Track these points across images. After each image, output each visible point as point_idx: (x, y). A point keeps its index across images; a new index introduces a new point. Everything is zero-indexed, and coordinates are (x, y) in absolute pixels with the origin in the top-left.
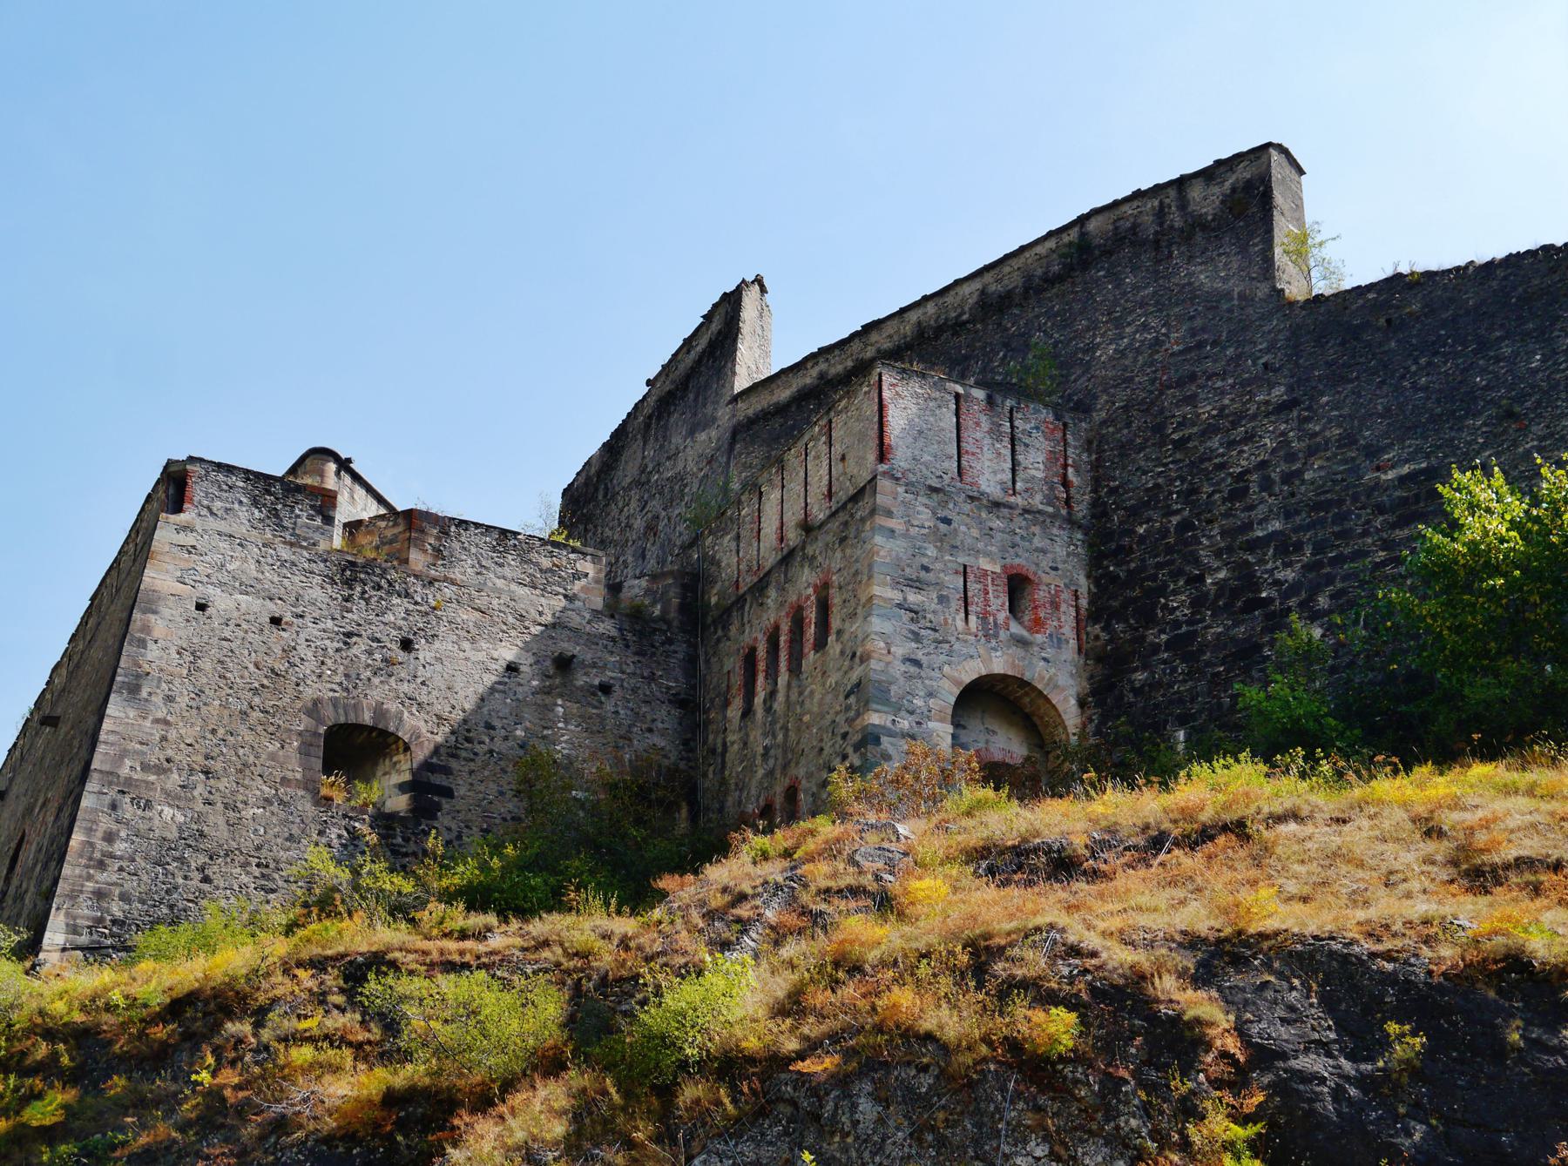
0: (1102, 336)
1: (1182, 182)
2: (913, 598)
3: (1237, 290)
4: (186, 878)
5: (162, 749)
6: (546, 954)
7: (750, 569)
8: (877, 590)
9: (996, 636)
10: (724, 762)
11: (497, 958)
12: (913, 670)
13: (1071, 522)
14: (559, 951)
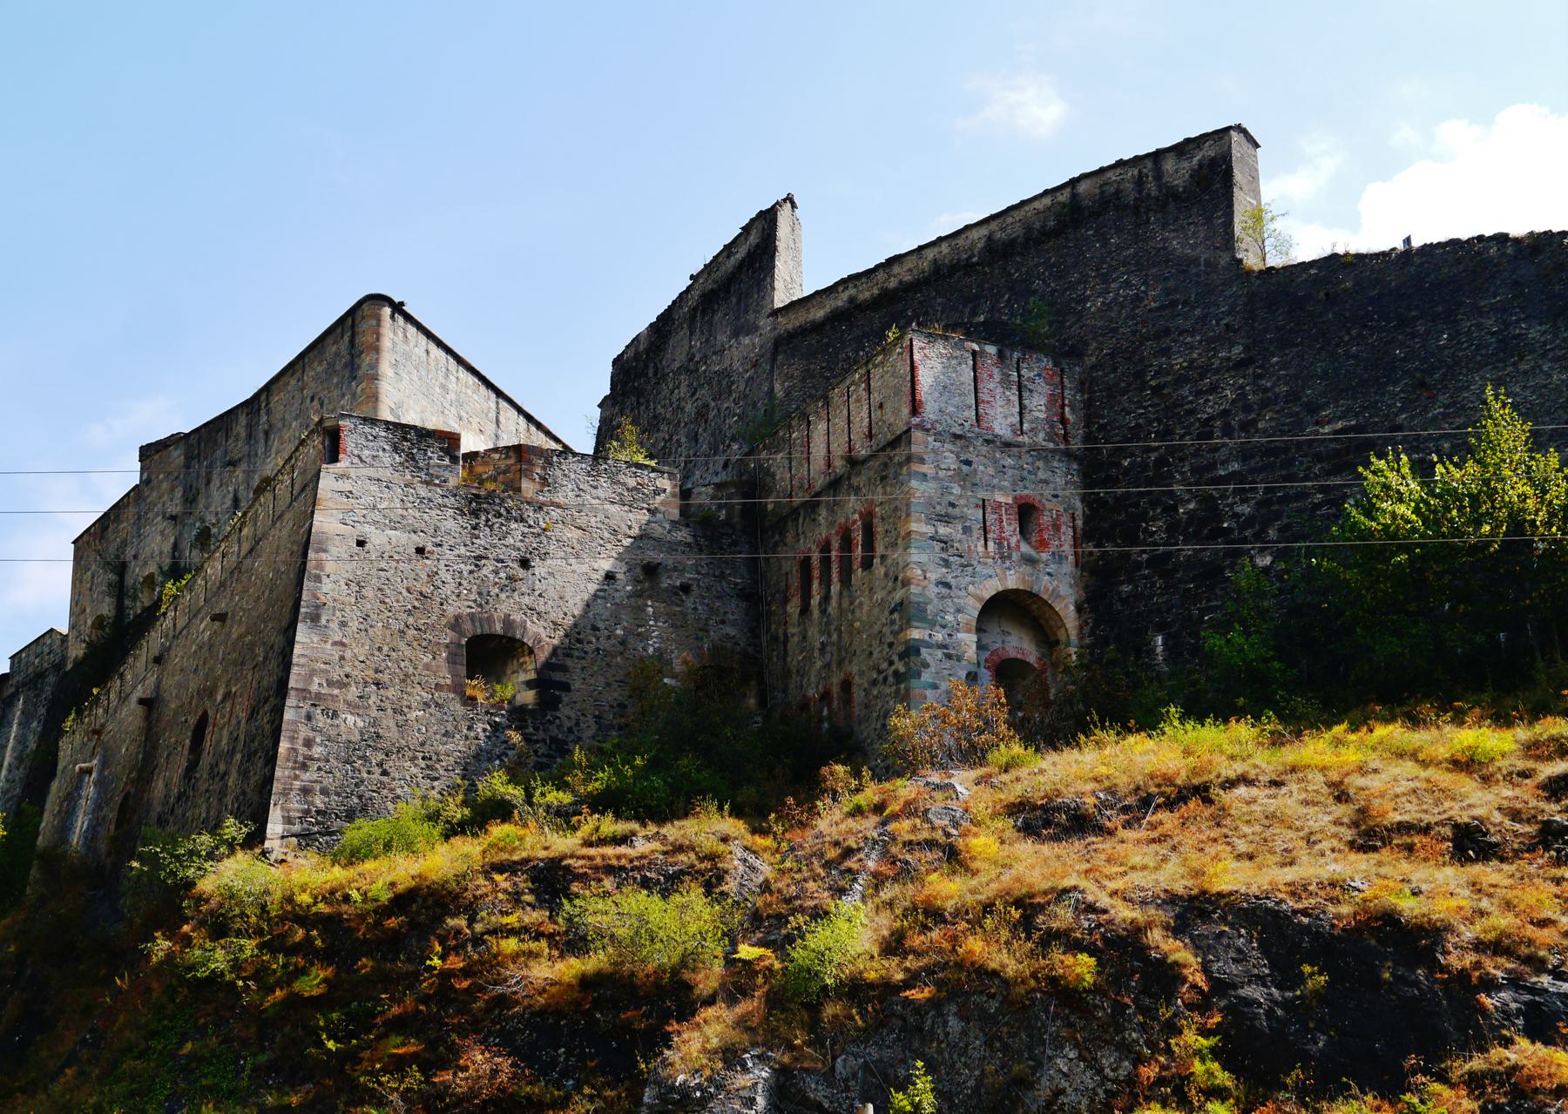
0: (1092, 288)
1: (1158, 155)
2: (943, 530)
3: (1203, 257)
4: (369, 772)
5: (342, 667)
6: (682, 857)
7: (801, 487)
8: (914, 526)
9: (1010, 557)
10: (786, 651)
11: (646, 862)
12: (945, 591)
13: (1069, 455)
14: (692, 855)
